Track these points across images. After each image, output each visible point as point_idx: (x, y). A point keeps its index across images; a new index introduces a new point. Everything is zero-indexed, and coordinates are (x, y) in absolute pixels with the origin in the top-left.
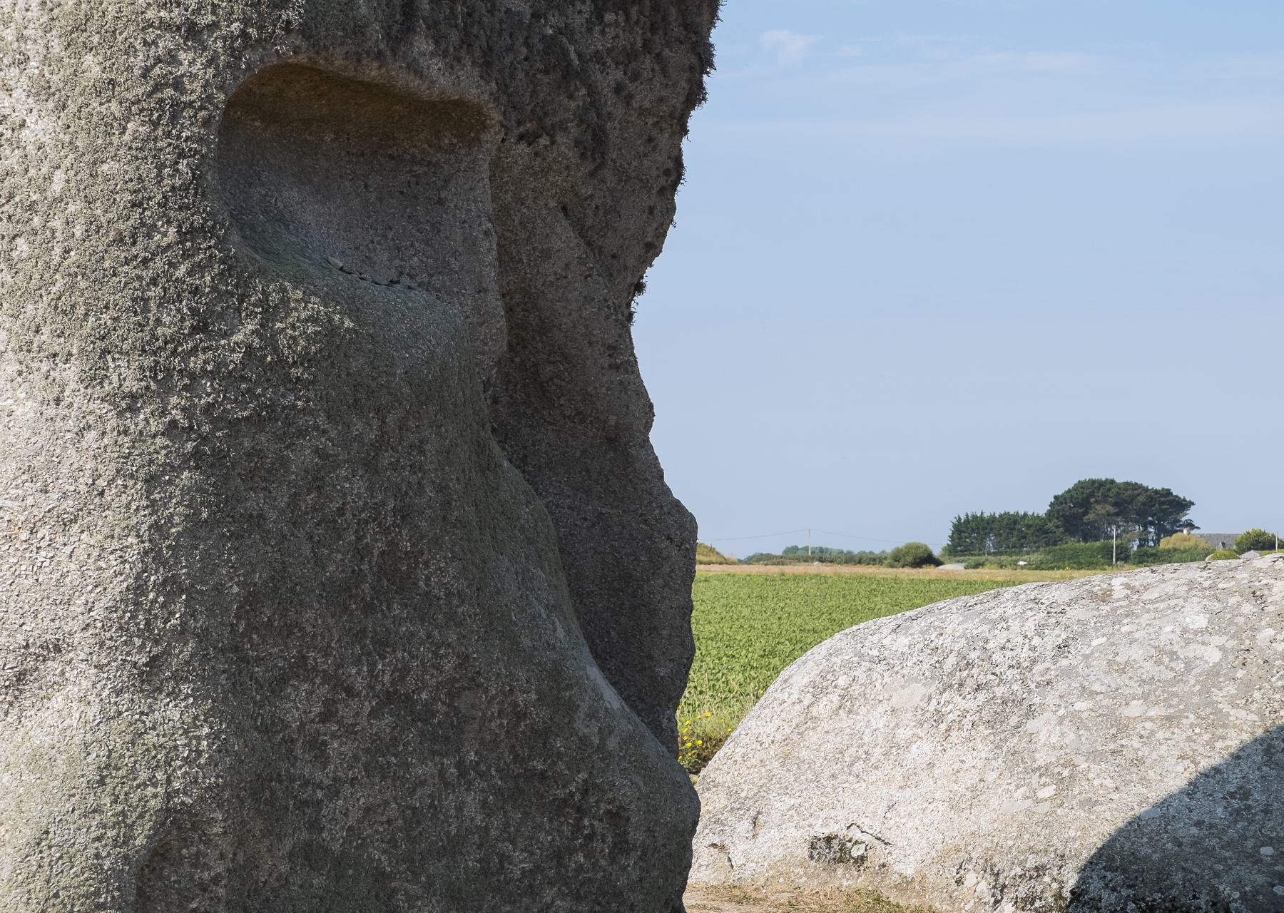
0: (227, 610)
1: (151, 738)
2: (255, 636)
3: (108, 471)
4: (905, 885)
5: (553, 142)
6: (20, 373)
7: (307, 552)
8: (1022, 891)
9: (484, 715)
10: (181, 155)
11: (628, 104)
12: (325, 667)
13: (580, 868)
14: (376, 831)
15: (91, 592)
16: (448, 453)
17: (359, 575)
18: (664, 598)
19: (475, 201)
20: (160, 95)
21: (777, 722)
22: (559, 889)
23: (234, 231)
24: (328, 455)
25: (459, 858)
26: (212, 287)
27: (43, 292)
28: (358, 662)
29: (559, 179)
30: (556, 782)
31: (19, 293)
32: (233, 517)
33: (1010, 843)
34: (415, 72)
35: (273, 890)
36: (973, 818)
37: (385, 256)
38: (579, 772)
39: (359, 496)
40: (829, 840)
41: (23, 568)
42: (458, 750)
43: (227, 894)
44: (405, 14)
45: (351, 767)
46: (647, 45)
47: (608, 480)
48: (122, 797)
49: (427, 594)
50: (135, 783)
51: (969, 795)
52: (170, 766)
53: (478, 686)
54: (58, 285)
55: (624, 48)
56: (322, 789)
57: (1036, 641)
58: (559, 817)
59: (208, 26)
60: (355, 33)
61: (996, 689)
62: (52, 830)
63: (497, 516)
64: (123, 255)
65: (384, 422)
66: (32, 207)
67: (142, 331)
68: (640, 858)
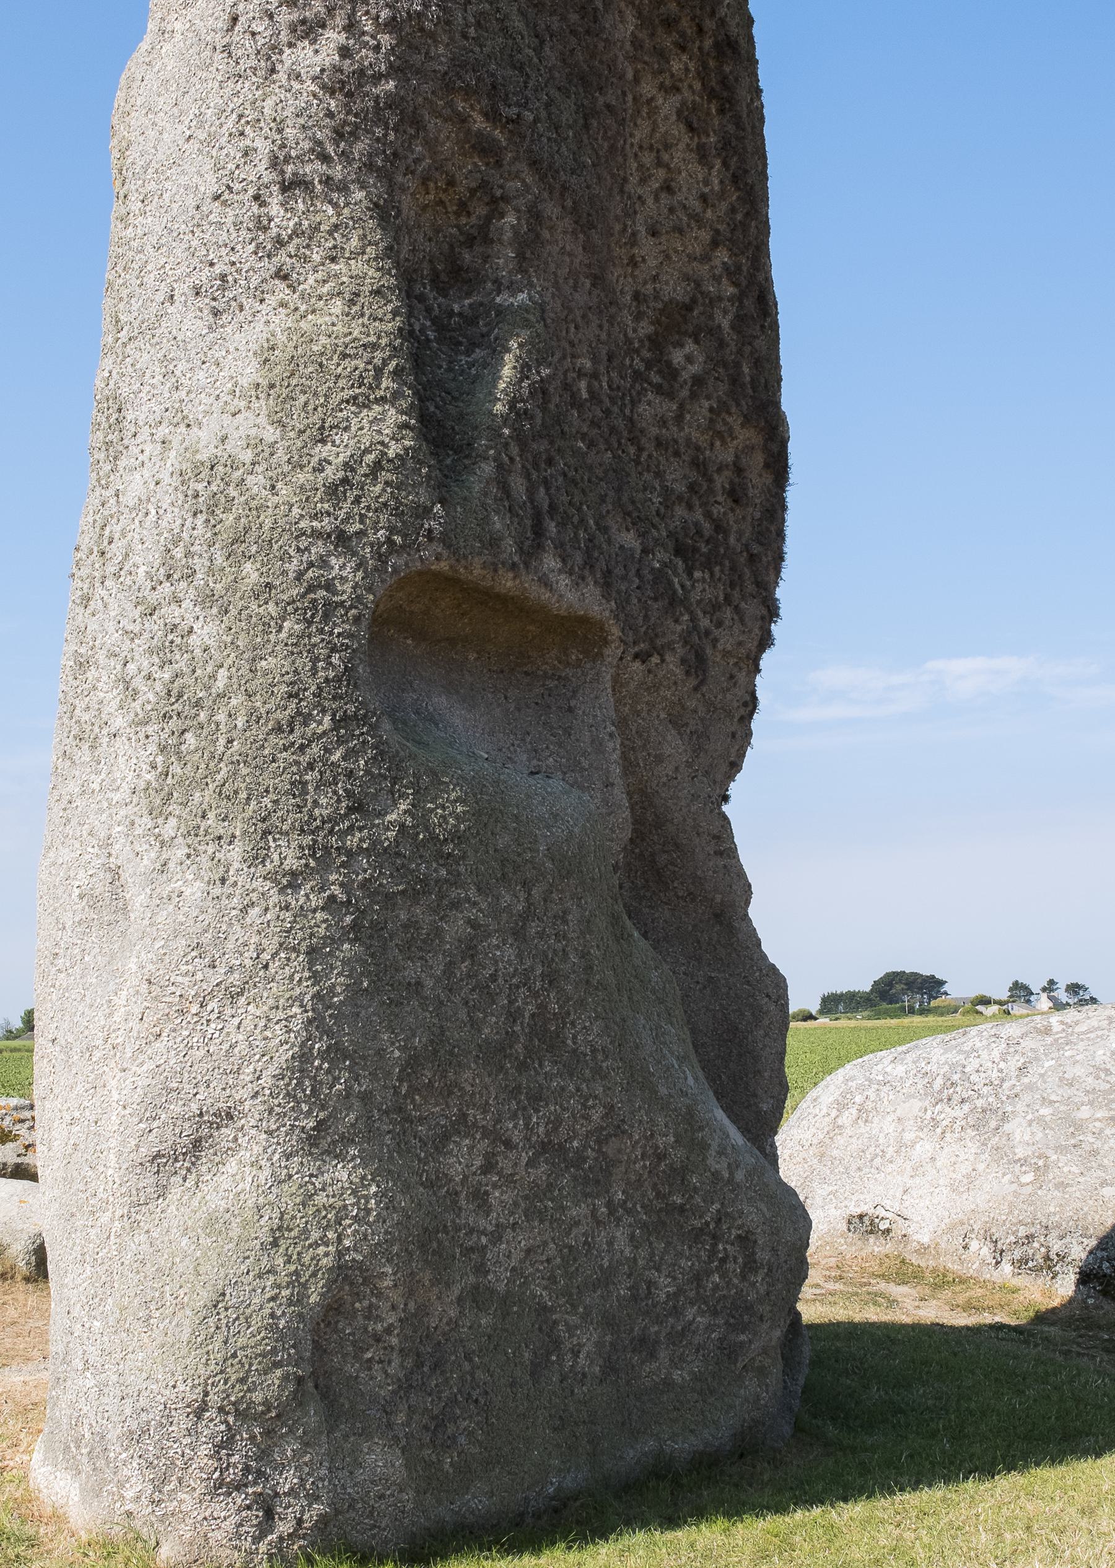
0: (389, 1073)
1: (321, 1199)
2: (417, 1097)
3: (271, 945)
4: (922, 1250)
5: (663, 661)
6: (189, 856)
7: (463, 1015)
8: (1017, 1254)
9: (629, 1158)
10: (334, 650)
11: (714, 647)
12: (484, 1123)
13: (716, 1287)
14: (538, 1270)
15: (258, 1061)
16: (588, 922)
17: (512, 1036)
18: (765, 1046)
19: (600, 708)
20: (312, 596)
21: (813, 1130)
22: (699, 1307)
23: (385, 719)
24: (480, 926)
25: (611, 1287)
26: (365, 771)
27: (209, 780)
28: (514, 1116)
29: (668, 694)
30: (693, 1214)
31: (187, 782)
32: (392, 985)
33: (1004, 1217)
34: (546, 585)
35: (444, 1334)
36: (971, 1199)
37: (525, 757)
38: (712, 1203)
39: (510, 962)
40: (861, 1217)
41: (195, 1040)
42: (607, 1192)
43: (400, 1342)
44: (536, 533)
45: (512, 1213)
46: (728, 599)
47: (716, 949)
48: (295, 1257)
49: (575, 1051)
50: (307, 1243)
51: (965, 1181)
52: (341, 1224)
53: (624, 1132)
54: (222, 773)
55: (710, 600)
56: (486, 1235)
57: (1002, 1065)
58: (697, 1244)
59: (357, 533)
60: (491, 545)
61: (976, 1102)
62: (228, 1292)
63: (632, 979)
64: (281, 742)
65: (529, 894)
66: (198, 704)
67: (301, 812)
68: (767, 1274)
